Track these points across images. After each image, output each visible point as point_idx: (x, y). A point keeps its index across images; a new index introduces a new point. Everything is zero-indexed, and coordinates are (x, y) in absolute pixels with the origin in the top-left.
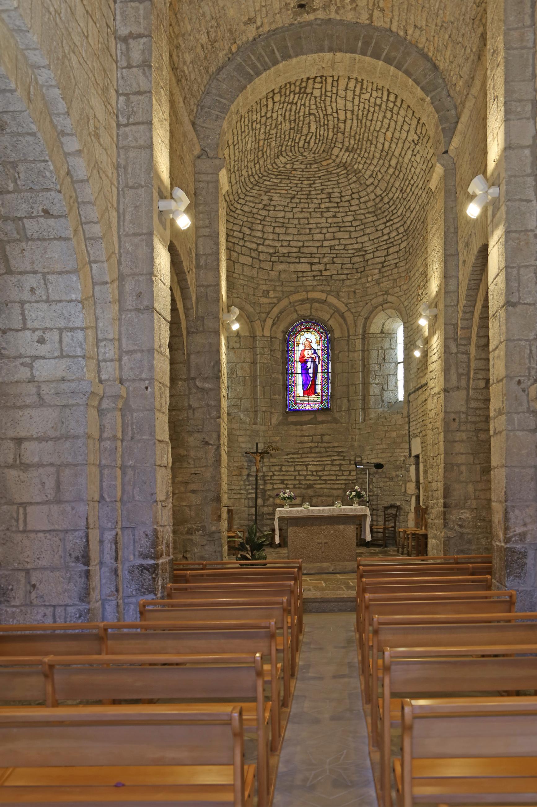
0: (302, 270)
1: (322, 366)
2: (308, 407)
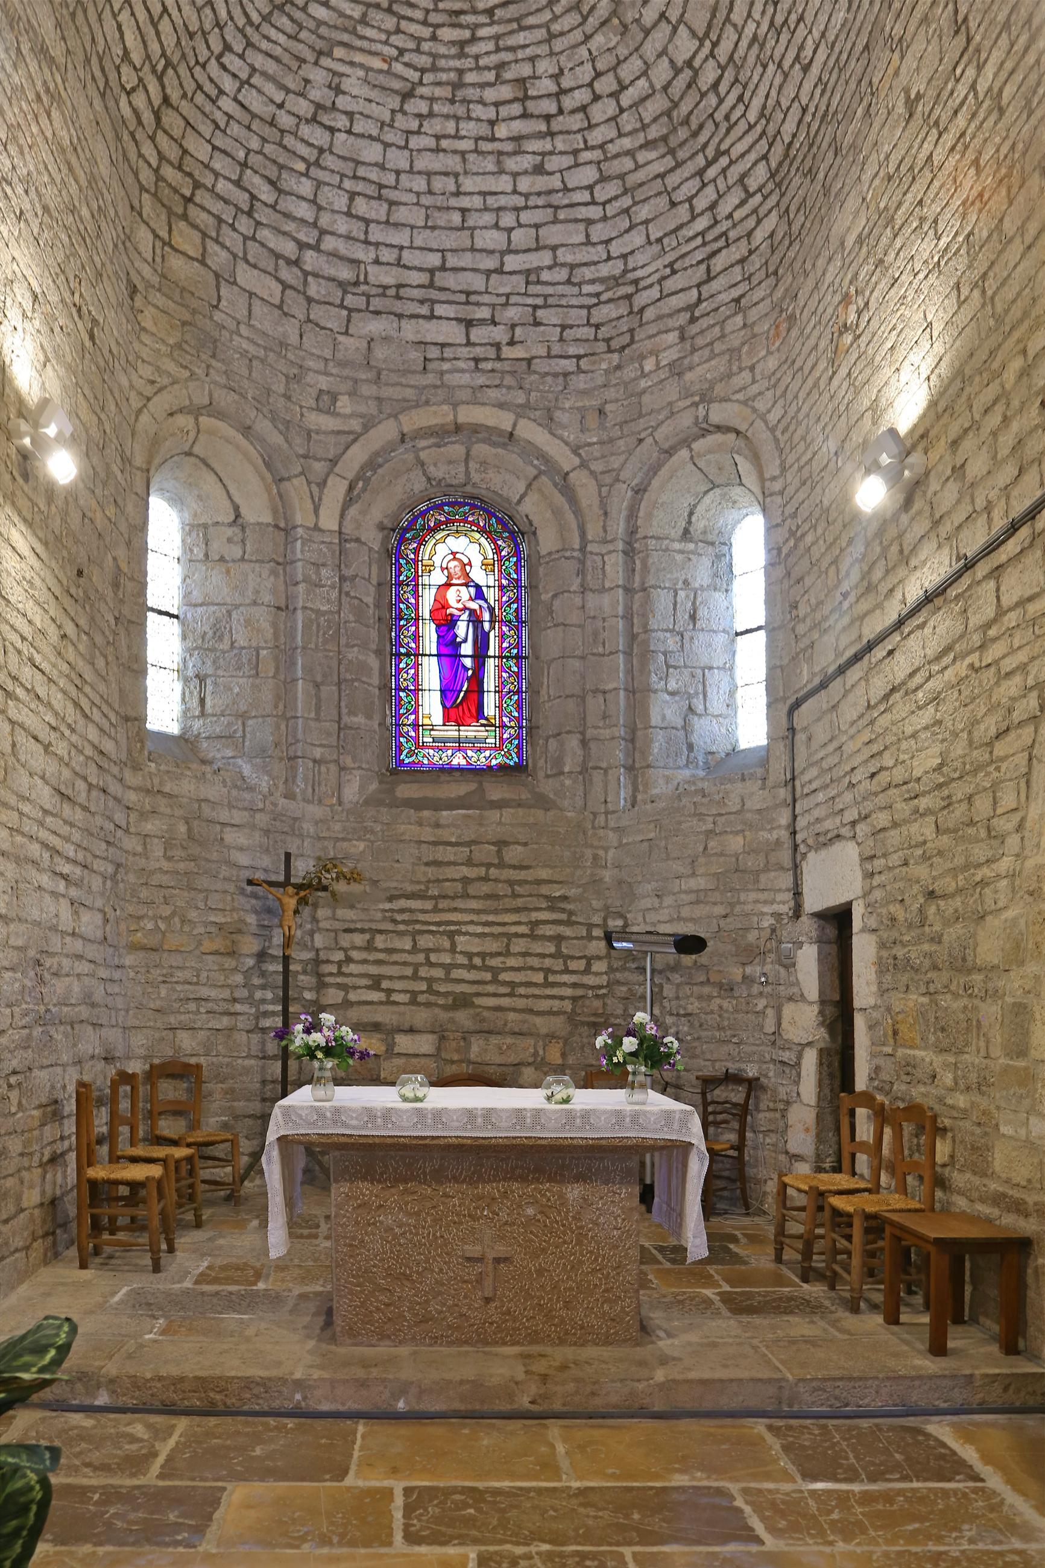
0: (441, 339)
1: (502, 637)
2: (459, 760)
